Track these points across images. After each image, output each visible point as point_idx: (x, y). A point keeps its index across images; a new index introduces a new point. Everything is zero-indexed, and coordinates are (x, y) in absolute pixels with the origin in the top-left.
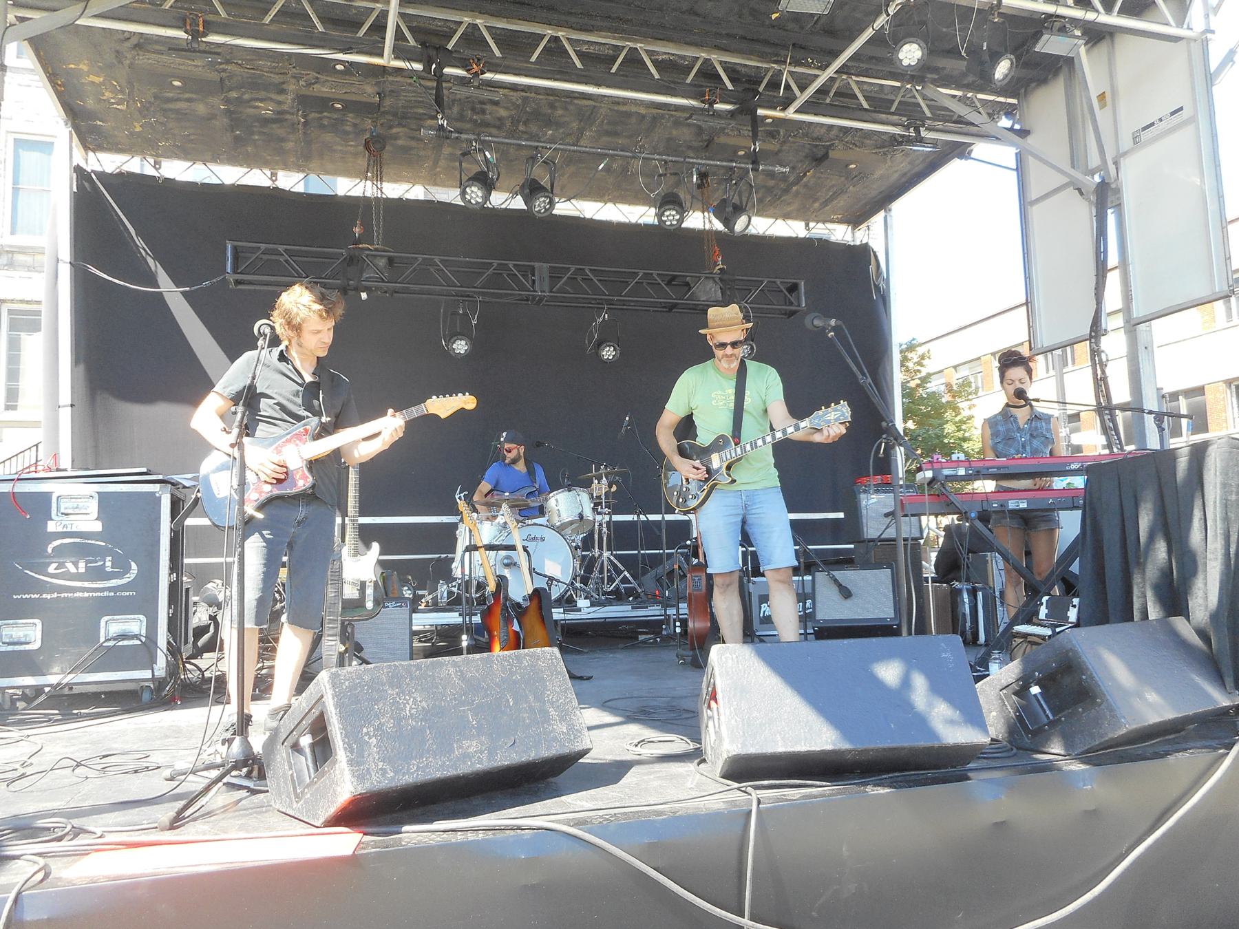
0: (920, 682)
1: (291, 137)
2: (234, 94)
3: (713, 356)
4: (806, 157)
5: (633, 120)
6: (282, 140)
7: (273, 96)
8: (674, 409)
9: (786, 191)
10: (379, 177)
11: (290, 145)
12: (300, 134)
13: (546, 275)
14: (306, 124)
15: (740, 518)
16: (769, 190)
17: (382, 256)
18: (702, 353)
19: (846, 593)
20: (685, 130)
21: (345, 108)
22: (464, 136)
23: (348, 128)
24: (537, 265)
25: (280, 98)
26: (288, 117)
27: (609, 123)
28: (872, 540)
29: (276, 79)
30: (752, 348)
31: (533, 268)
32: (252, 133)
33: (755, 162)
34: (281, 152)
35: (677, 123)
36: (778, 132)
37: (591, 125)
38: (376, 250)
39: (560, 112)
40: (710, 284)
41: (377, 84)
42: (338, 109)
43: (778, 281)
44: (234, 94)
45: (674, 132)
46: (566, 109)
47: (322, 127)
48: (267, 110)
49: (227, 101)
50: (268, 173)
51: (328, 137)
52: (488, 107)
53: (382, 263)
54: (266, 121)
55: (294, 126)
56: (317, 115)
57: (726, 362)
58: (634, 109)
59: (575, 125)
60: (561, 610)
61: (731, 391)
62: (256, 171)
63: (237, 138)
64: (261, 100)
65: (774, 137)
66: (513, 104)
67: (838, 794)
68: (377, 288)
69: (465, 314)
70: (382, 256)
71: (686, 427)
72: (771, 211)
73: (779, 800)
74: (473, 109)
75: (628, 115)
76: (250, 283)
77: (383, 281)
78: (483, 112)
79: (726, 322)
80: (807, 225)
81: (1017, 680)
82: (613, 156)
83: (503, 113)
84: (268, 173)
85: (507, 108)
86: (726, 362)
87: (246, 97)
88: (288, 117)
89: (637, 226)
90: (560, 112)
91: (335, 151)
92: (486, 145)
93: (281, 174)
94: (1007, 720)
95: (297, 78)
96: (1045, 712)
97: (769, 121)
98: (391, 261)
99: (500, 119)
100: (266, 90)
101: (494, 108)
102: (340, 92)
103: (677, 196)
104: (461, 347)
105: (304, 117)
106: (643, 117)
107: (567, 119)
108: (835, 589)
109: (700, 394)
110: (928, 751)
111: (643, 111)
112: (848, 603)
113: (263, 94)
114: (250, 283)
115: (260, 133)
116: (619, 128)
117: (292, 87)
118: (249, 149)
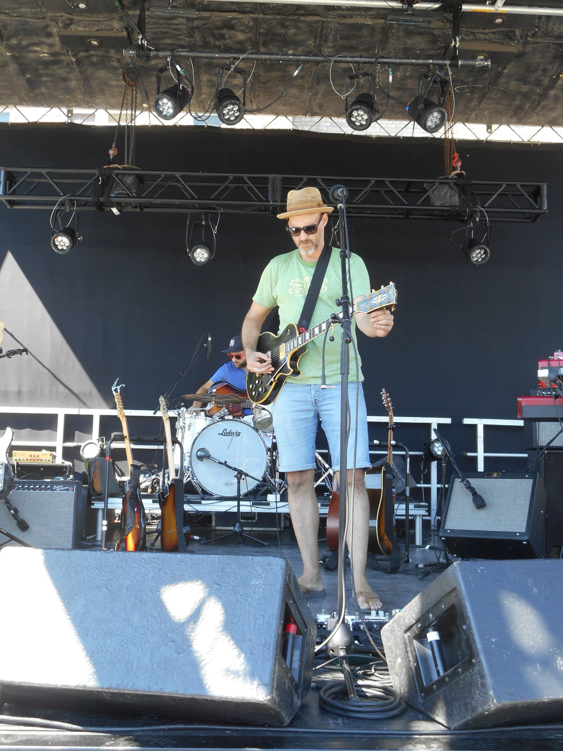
0: (214, 612)
1: (72, 76)
2: (14, 42)
3: (292, 247)
4: (555, 58)
5: (365, 33)
6: (65, 80)
7: (45, 40)
8: (260, 302)
9: (544, 95)
10: (134, 106)
11: (73, 84)
12: (77, 73)
13: (279, 186)
14: (78, 62)
15: (311, 414)
16: (526, 96)
17: (130, 175)
18: (281, 241)
19: (480, 503)
20: (419, 39)
21: (101, 44)
22: (161, 54)
23: (115, 64)
24: (270, 176)
25: (50, 41)
26: (63, 58)
27: (341, 38)
28: (541, 448)
29: (40, 24)
30: (486, 253)
31: (132, 165)
32: (40, 76)
33: (454, 58)
34: (68, 91)
35: (409, 33)
36: (513, 32)
37: (326, 41)
38: (124, 169)
39: (292, 31)
40: (446, 190)
41: (121, 19)
42: (94, 46)
43: (518, 184)
44: (14, 42)
45: (409, 42)
46: (298, 28)
47: (93, 64)
48: (44, 54)
49: (10, 48)
50: (65, 110)
51: (102, 74)
52: (225, 31)
53: (129, 180)
54: (47, 64)
55: (69, 64)
56: (86, 54)
57: (307, 251)
58: (360, 20)
59: (311, 42)
60: (248, 503)
61: (308, 280)
62: (56, 110)
63: (28, 81)
64: (37, 44)
65: (511, 39)
66: (247, 26)
67: (75, 743)
68: (127, 204)
69: (207, 225)
70: (130, 175)
71: (272, 319)
72: (535, 118)
73: (72, 736)
74: (213, 35)
75: (358, 27)
76: (24, 203)
77: (129, 197)
78: (222, 37)
79: (303, 207)
80: (489, 127)
81: (417, 621)
82: (304, 62)
83: (241, 36)
84: (65, 110)
85: (242, 31)
86: (307, 251)
87: (24, 43)
88: (63, 58)
89: (396, 139)
90: (292, 31)
91: (111, 86)
92: (176, 60)
93: (77, 111)
94: (409, 669)
95: (55, 20)
96: (436, 666)
97: (499, 21)
98: (140, 179)
99: (240, 42)
100: (37, 35)
101: (232, 32)
102: (92, 30)
103: (371, 97)
104: (201, 255)
105: (74, 56)
106: (372, 29)
107: (301, 37)
108: (470, 497)
109: (282, 284)
110: (193, 702)
111: (369, 22)
112: (482, 512)
113: (35, 39)
114: (24, 203)
115: (47, 75)
116: (354, 42)
117: (55, 30)
118: (43, 90)
